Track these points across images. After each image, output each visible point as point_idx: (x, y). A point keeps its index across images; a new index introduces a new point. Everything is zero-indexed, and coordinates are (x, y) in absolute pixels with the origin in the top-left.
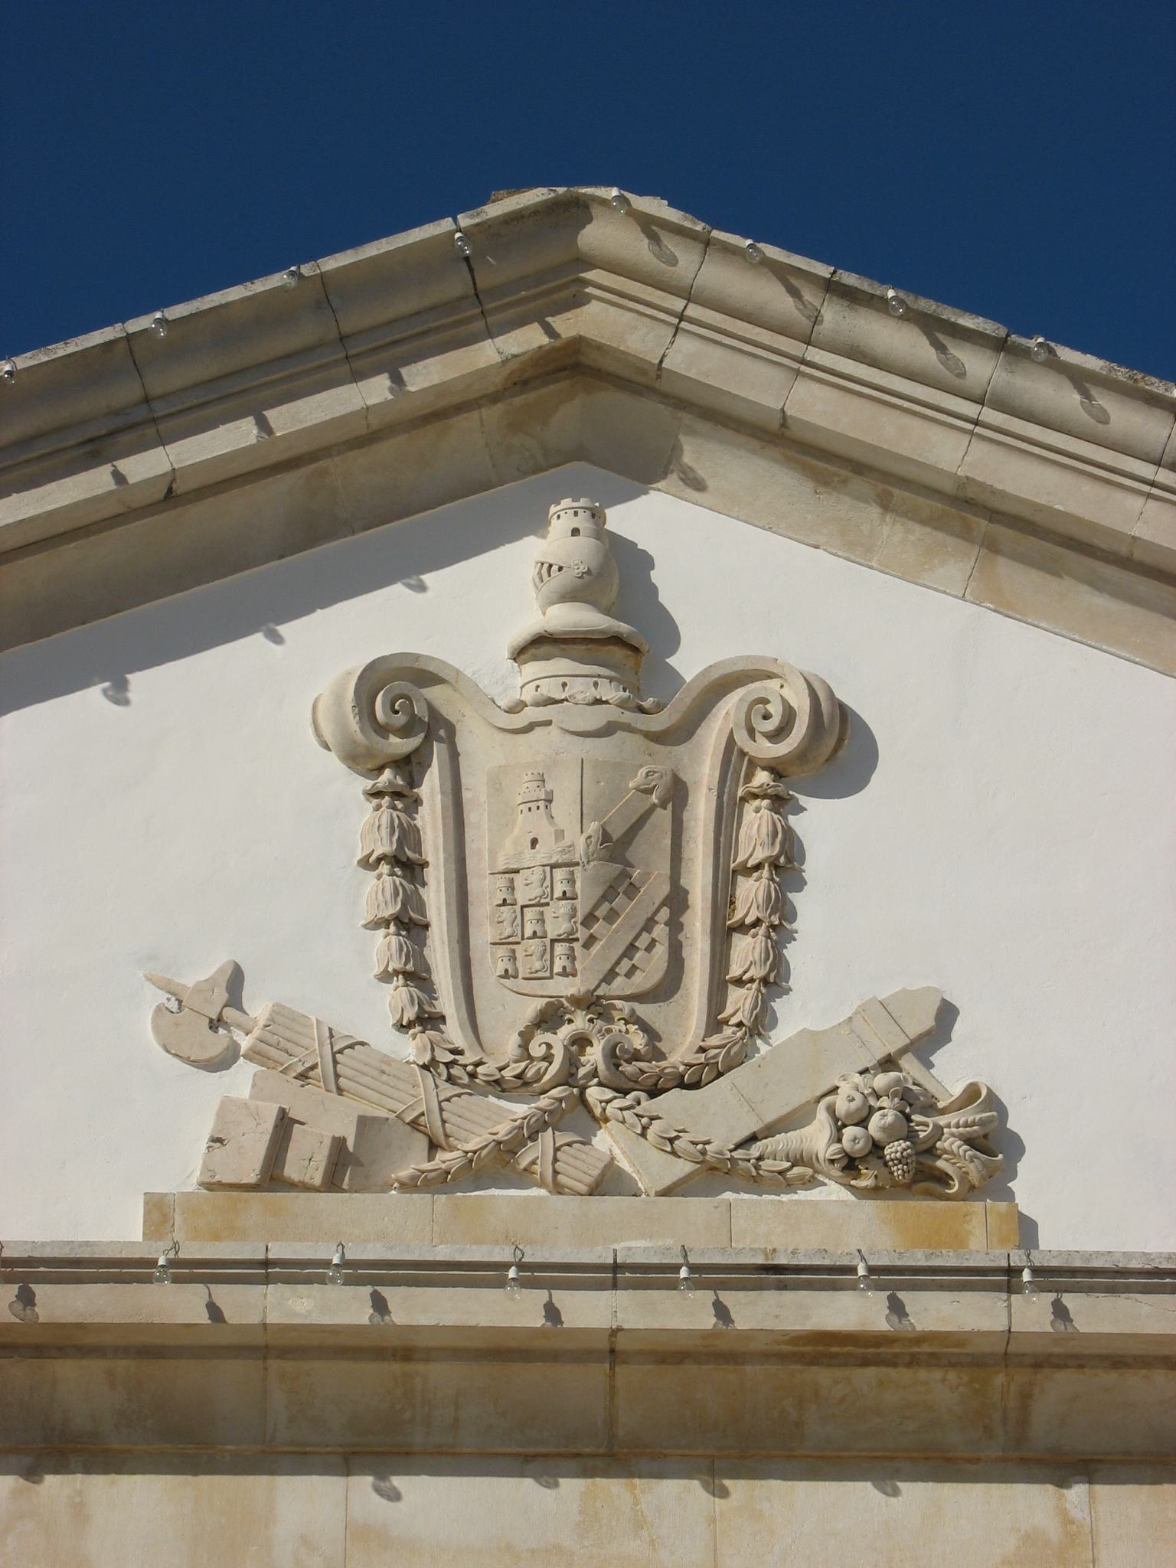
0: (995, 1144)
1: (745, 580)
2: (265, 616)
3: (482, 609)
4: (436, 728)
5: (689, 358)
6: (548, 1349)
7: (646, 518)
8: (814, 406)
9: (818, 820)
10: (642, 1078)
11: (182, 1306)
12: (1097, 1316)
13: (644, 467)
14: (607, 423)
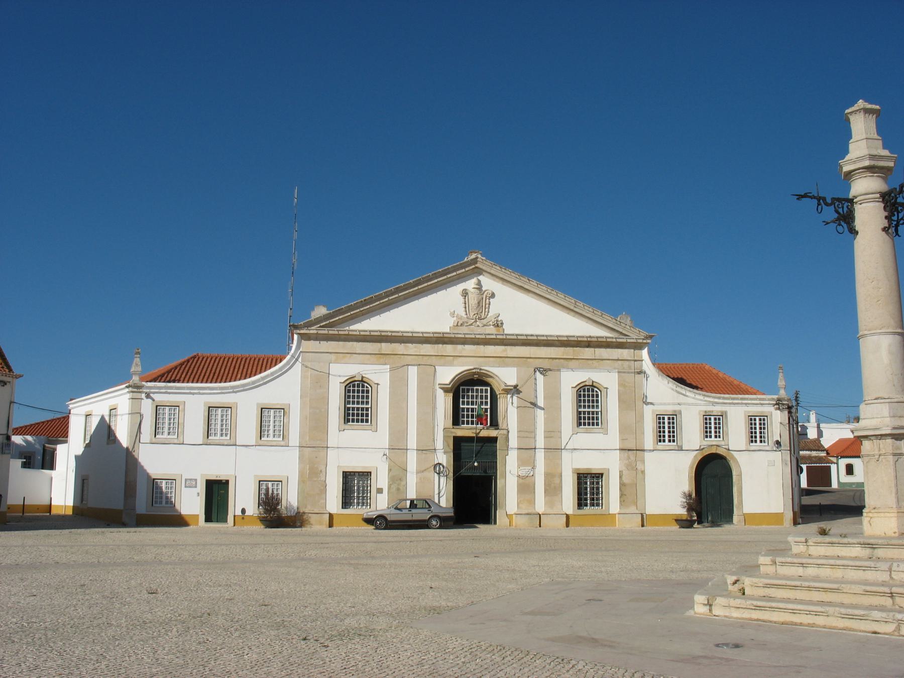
0: (502, 324)
1: (488, 283)
2: (455, 285)
3: (470, 284)
4: (467, 294)
5: (484, 268)
6: (381, 336)
7: (481, 278)
8: (492, 272)
9: (491, 300)
10: (480, 319)
11: (453, 336)
12: (508, 337)
13: (480, 274)
14: (478, 272)
